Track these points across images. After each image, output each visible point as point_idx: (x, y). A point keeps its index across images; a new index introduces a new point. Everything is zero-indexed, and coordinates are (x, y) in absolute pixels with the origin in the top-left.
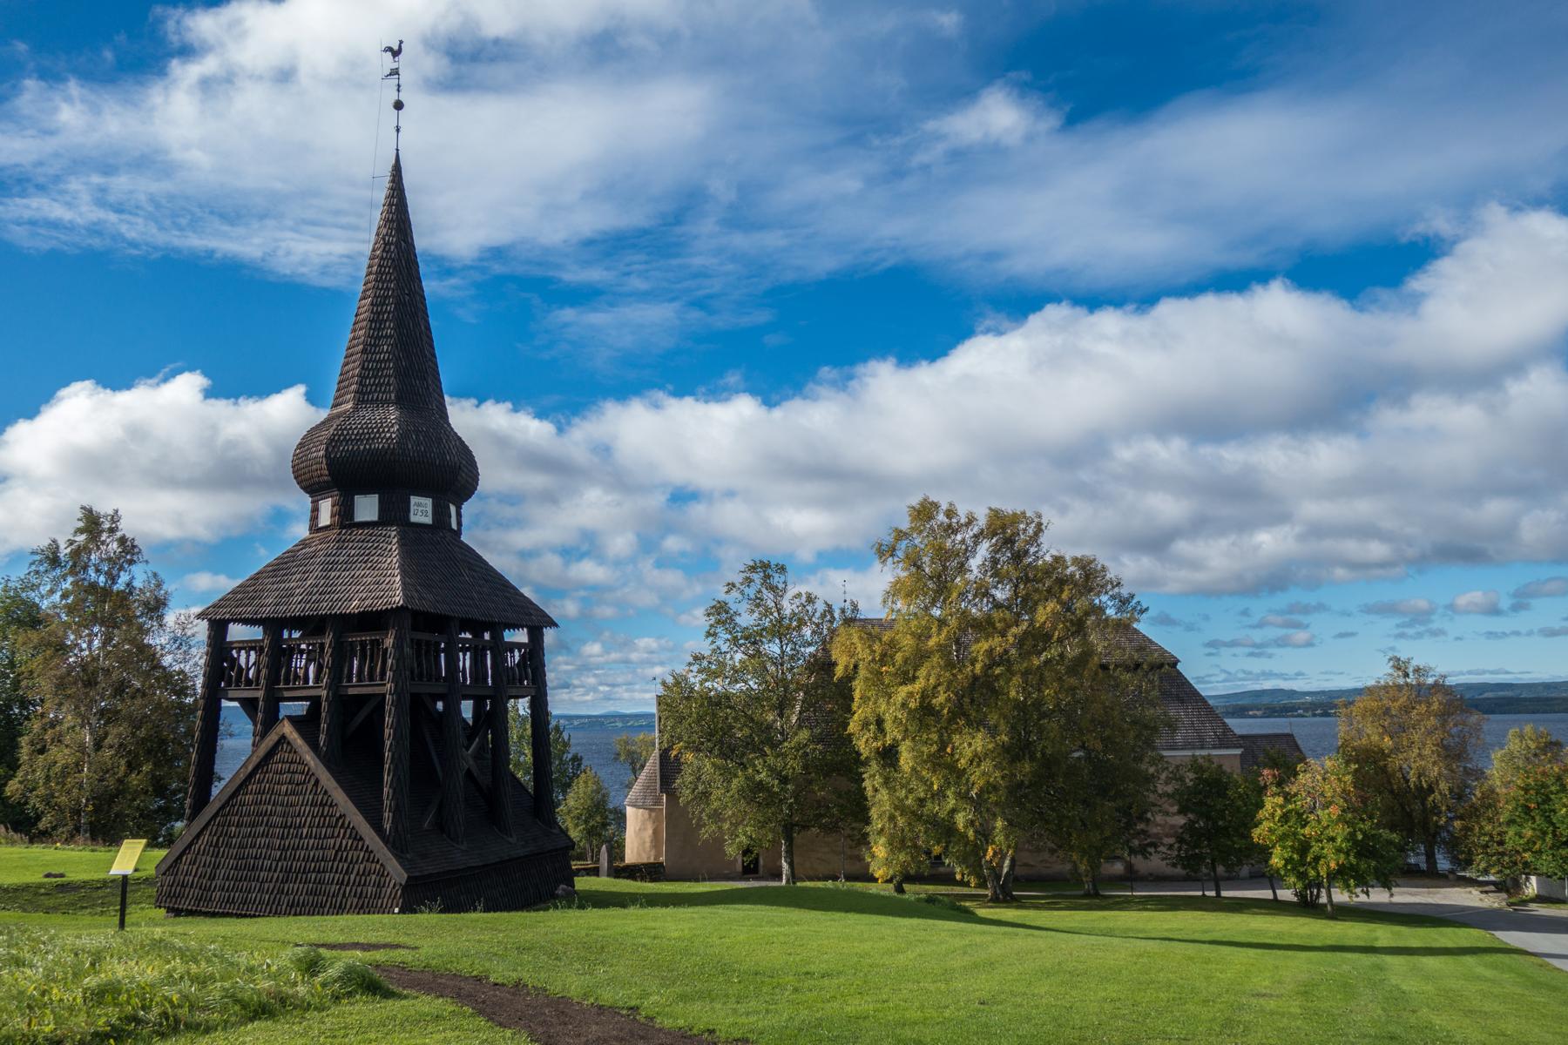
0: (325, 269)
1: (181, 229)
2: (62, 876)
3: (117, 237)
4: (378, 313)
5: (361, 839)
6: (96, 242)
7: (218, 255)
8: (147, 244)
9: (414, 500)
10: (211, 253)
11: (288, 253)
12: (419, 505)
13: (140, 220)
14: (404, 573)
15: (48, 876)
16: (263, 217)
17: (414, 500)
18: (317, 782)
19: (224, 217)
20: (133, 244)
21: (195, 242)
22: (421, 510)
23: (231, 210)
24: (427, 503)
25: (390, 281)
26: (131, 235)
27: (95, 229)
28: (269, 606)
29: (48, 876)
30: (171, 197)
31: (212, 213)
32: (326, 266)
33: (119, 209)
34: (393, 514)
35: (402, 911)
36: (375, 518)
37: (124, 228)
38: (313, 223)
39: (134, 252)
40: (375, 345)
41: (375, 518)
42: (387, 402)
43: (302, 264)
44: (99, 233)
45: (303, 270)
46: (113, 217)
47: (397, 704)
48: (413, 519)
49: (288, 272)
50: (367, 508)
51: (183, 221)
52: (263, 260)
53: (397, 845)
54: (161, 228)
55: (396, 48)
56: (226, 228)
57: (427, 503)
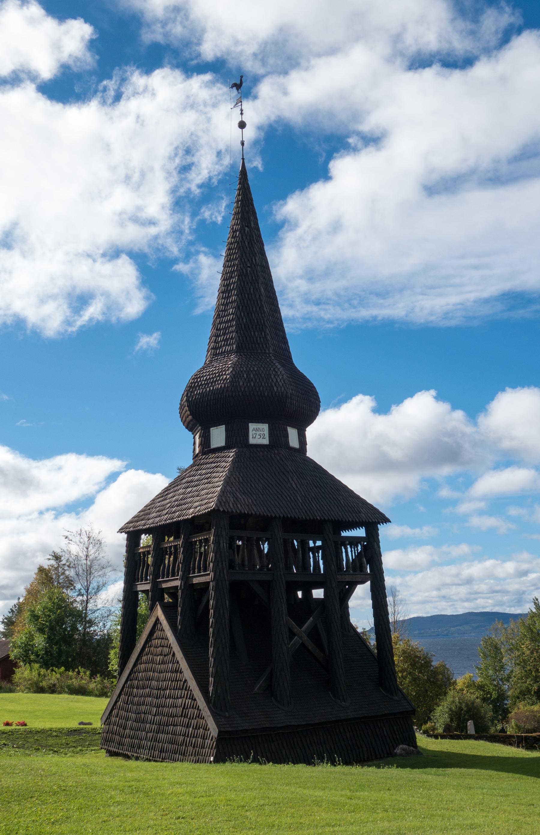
0: (446, 315)
1: (355, 307)
2: (90, 724)
3: (320, 319)
4: (228, 285)
5: (195, 700)
6: (309, 325)
7: (380, 318)
8: (337, 320)
9: (252, 426)
10: (375, 318)
11: (422, 309)
12: (257, 430)
13: (331, 307)
14: (227, 481)
15: (81, 723)
16: (401, 290)
17: (252, 426)
18: (174, 655)
19: (379, 295)
20: (329, 322)
21: (365, 313)
22: (259, 434)
23: (383, 292)
24: (264, 428)
25: (236, 259)
26: (327, 316)
27: (306, 318)
28: (154, 521)
29: (80, 724)
30: (346, 289)
31: (371, 293)
32: (447, 313)
33: (318, 303)
34: (237, 438)
35: (216, 761)
36: (223, 444)
37: (322, 314)
38: (432, 287)
39: (331, 326)
40: (225, 310)
41: (223, 444)
42: (230, 352)
43: (432, 315)
44: (309, 319)
45: (433, 318)
46: (315, 309)
47: (216, 589)
48: (252, 441)
49: (422, 321)
50: (218, 436)
51: (355, 302)
52: (406, 316)
53: (217, 706)
54: (343, 310)
55: (238, 82)
56: (381, 301)
57: (264, 428)
